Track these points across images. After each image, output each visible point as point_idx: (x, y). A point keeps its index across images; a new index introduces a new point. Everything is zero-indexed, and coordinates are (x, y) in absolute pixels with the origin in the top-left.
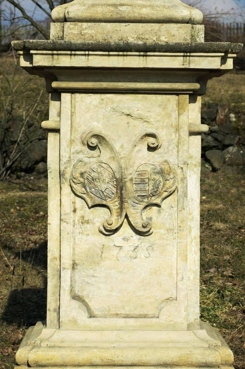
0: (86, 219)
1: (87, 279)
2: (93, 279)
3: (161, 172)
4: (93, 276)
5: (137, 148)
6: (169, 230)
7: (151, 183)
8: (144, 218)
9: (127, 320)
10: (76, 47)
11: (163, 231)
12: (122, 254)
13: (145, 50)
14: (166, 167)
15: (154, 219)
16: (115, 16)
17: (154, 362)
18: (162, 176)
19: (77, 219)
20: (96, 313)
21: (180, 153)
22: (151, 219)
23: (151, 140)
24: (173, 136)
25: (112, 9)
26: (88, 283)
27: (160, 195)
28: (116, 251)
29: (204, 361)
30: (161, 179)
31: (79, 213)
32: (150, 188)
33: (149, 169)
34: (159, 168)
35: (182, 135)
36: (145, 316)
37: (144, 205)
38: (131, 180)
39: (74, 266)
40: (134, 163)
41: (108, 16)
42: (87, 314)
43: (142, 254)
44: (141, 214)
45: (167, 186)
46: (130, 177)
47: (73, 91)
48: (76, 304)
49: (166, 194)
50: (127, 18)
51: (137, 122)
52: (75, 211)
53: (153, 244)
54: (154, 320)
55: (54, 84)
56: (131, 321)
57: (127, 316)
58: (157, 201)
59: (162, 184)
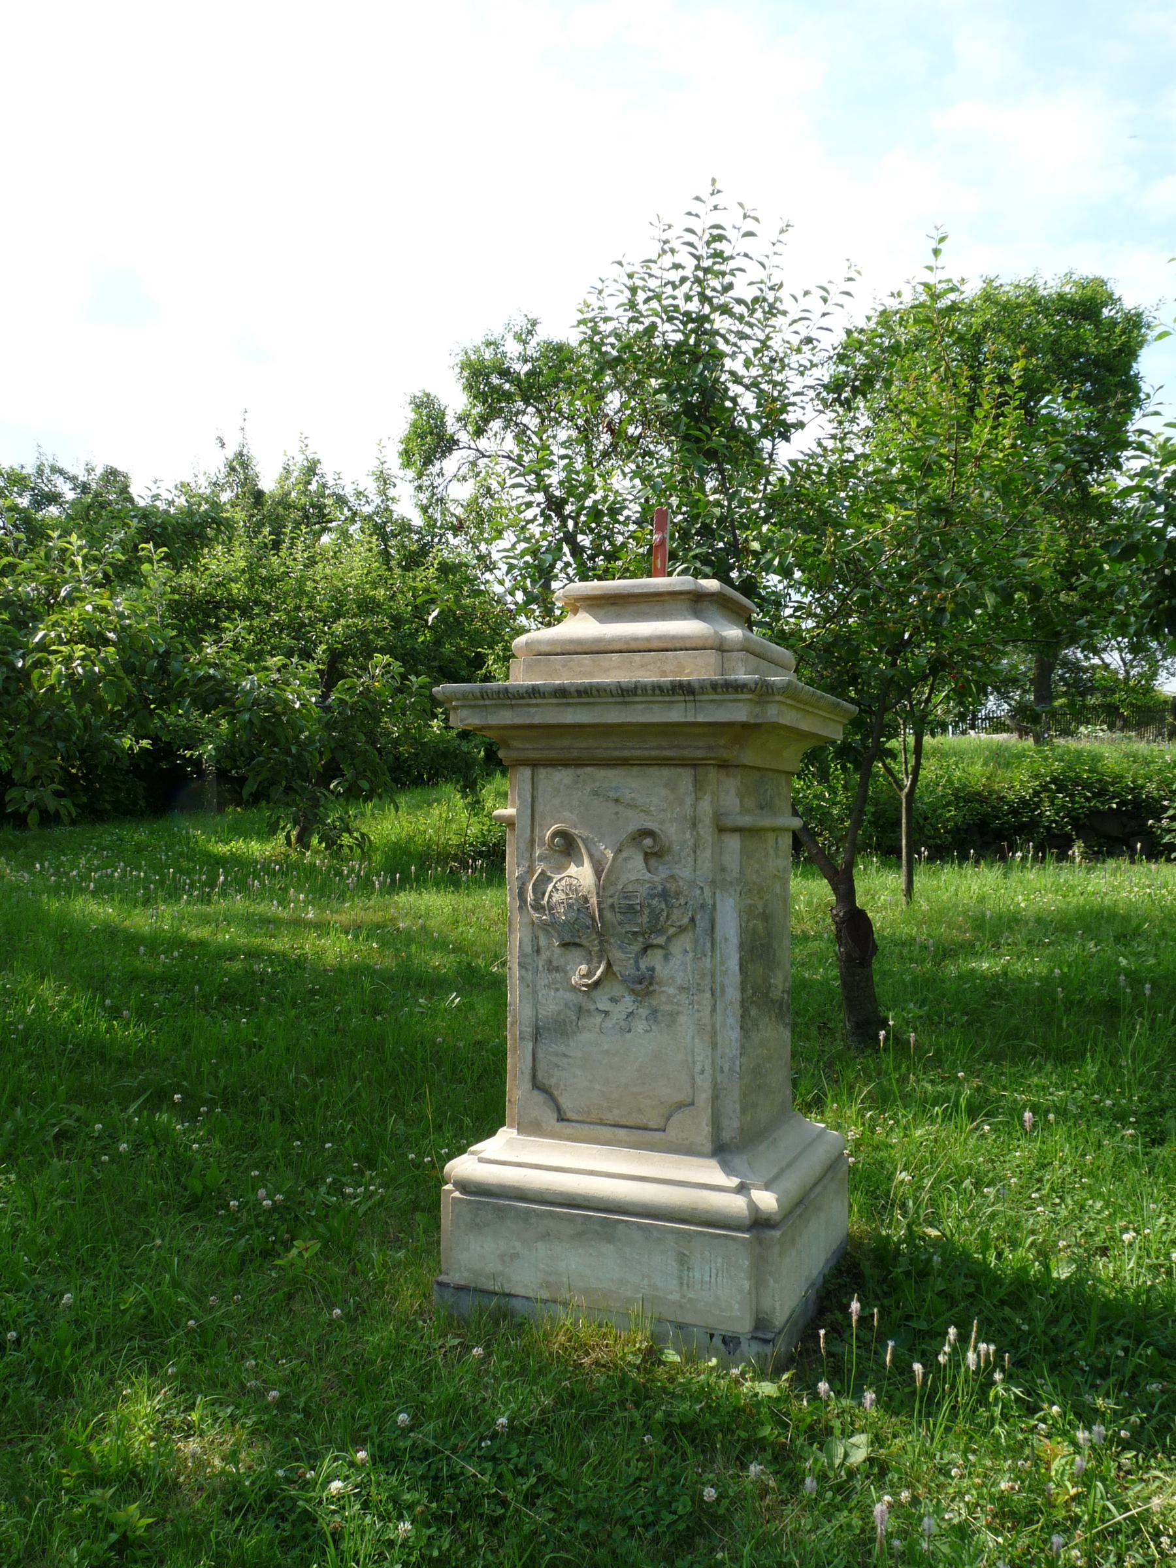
0: (555, 964)
1: (554, 1059)
2: (565, 1060)
3: (664, 895)
4: (565, 1056)
5: (625, 854)
6: (682, 989)
8: (643, 966)
10: (151, 675)
11: (671, 990)
12: (609, 1024)
14: (671, 887)
15: (658, 968)
18: (666, 901)
19: (541, 964)
20: (570, 1115)
21: (699, 862)
22: (652, 969)
23: (648, 842)
24: (688, 836)
26: (557, 1066)
28: (598, 1019)
31: (545, 955)
33: (643, 890)
34: (660, 888)
35: (702, 832)
39: (537, 1035)
40: (618, 879)
42: (555, 1115)
43: (640, 1026)
44: (637, 962)
45: (674, 917)
51: (630, 813)
52: (538, 951)
53: (656, 1011)
54: (658, 1135)
58: (661, 940)
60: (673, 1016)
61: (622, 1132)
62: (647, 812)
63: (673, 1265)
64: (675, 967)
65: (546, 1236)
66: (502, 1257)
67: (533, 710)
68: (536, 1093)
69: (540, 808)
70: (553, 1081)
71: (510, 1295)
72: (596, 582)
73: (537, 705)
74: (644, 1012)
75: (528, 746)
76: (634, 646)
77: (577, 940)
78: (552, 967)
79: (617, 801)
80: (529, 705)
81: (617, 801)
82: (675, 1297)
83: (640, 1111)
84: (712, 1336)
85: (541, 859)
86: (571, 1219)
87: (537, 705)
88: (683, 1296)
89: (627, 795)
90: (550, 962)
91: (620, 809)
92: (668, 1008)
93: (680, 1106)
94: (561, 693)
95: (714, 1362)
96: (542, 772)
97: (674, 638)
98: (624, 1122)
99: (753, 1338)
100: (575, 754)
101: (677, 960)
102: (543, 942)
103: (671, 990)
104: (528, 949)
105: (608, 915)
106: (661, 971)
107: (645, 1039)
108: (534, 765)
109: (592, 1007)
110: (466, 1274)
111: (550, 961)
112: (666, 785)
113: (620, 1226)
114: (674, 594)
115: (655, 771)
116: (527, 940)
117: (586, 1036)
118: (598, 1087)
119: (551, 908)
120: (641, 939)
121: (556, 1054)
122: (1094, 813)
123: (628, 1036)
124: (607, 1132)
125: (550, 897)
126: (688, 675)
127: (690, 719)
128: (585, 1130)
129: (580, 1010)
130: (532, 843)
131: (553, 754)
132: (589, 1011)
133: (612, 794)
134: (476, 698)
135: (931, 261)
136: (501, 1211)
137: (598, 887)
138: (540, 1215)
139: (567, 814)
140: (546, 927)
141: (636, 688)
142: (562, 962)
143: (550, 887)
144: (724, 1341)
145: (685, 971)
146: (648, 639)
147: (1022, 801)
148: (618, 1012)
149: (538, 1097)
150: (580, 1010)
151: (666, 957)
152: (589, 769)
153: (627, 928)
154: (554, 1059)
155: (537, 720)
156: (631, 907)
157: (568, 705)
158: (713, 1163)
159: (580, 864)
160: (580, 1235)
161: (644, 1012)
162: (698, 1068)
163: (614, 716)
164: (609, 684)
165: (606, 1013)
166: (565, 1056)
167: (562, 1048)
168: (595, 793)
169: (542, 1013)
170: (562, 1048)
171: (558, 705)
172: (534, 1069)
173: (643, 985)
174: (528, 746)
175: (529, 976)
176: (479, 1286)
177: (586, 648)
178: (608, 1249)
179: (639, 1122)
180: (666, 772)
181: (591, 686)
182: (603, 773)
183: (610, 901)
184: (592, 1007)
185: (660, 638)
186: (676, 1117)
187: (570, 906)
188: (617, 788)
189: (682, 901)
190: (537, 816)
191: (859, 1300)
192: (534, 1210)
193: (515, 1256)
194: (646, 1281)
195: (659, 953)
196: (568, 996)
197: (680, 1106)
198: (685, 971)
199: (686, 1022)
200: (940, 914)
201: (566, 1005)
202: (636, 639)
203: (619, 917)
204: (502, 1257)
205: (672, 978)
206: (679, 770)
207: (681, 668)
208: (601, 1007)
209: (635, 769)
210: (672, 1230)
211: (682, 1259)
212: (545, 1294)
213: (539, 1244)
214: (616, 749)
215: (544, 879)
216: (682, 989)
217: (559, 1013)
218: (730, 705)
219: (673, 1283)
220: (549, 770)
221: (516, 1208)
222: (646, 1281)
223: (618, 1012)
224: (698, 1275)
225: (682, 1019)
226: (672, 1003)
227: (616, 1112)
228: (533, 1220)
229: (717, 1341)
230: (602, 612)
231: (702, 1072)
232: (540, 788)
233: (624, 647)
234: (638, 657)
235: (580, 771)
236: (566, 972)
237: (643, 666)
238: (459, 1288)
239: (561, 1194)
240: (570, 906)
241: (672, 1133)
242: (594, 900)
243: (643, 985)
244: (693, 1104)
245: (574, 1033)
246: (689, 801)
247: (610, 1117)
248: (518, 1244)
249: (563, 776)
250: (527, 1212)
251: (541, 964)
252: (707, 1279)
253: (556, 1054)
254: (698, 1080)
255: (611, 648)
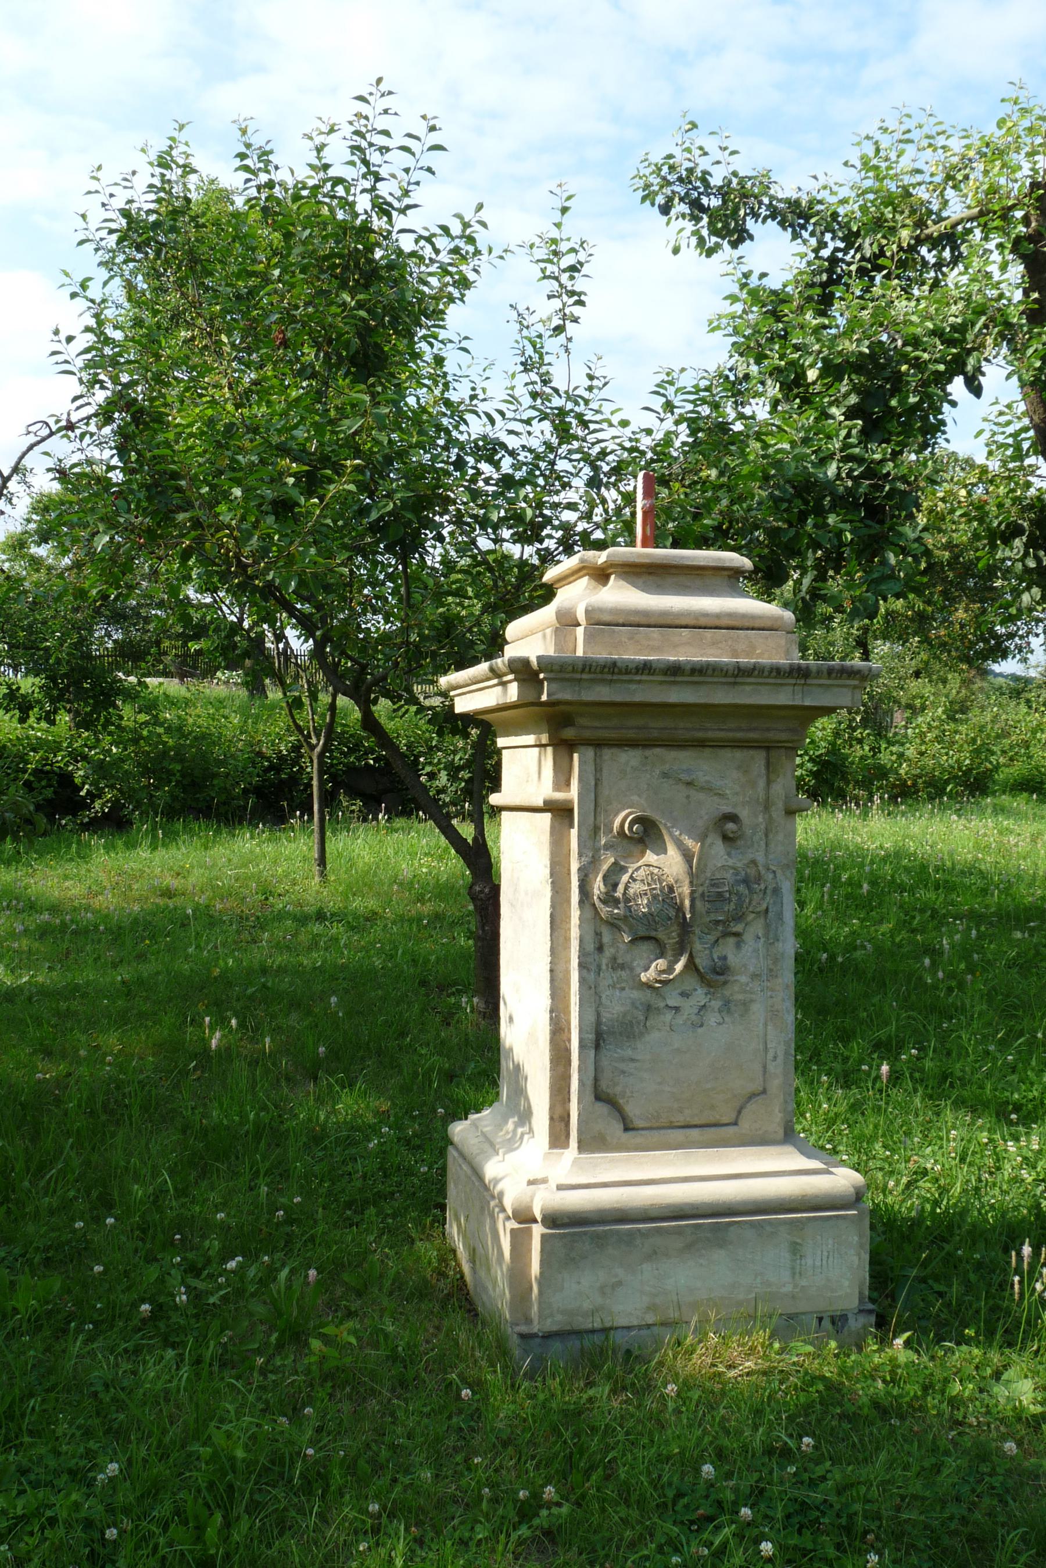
0: (620, 961)
1: (622, 1066)
2: (632, 1065)
4: (632, 1060)
6: (755, 976)
12: (680, 1020)
19: (604, 961)
21: (772, 846)
24: (761, 820)
28: (668, 1016)
31: (609, 952)
35: (774, 815)
43: (712, 1019)
45: (754, 903)
51: (701, 796)
54: (731, 1130)
60: (746, 1005)
61: (695, 1133)
62: (721, 796)
63: (786, 1256)
64: (746, 957)
65: (652, 1256)
66: (602, 1290)
67: (633, 687)
68: (599, 1104)
69: (605, 792)
70: (618, 1089)
71: (605, 1331)
72: (734, 555)
73: (639, 682)
74: (716, 1004)
75: (597, 724)
76: (703, 621)
77: (653, 934)
78: (616, 965)
79: (689, 784)
80: (630, 681)
81: (689, 784)
82: (788, 1288)
83: (713, 1107)
84: (820, 1319)
85: (608, 847)
86: (679, 1231)
87: (639, 682)
88: (795, 1286)
89: (701, 778)
90: (614, 959)
91: (692, 792)
92: (740, 997)
93: (753, 1096)
94: (674, 670)
95: (833, 1344)
96: (607, 753)
97: (744, 616)
98: (696, 1121)
99: (861, 1311)
100: (655, 734)
101: (748, 948)
102: (606, 939)
103: (743, 979)
104: (591, 947)
105: (699, 904)
106: (733, 960)
107: (718, 1032)
108: (598, 744)
109: (662, 1005)
110: (559, 1317)
111: (614, 959)
112: (739, 768)
113: (732, 1228)
114: (718, 570)
115: (727, 753)
116: (590, 938)
117: (654, 1036)
118: (667, 1089)
119: (627, 899)
120: (720, 928)
121: (623, 1060)
122: (351, 769)
123: (700, 1030)
124: (678, 1135)
125: (626, 888)
126: (760, 656)
127: (798, 702)
128: (655, 1136)
129: (649, 1008)
130: (596, 830)
131: (631, 734)
132: (658, 1009)
133: (685, 777)
134: (574, 671)
135: (557, 217)
136: (600, 1241)
137: (691, 874)
138: (644, 1234)
139: (635, 798)
140: (613, 924)
141: (754, 669)
142: (628, 958)
143: (625, 878)
144: (833, 1323)
145: (758, 958)
146: (718, 616)
147: (281, 758)
148: (689, 1007)
149: (602, 1108)
150: (649, 1008)
151: (738, 946)
152: (657, 751)
153: (713, 917)
154: (622, 1066)
155: (638, 698)
156: (720, 895)
157: (674, 683)
158: (790, 1149)
159: (662, 850)
160: (689, 1247)
161: (716, 1004)
162: (770, 1055)
163: (722, 696)
164: (727, 664)
165: (677, 1009)
166: (632, 1060)
167: (629, 1053)
168: (665, 775)
169: (606, 1016)
170: (629, 1053)
171: (661, 683)
172: (596, 1080)
173: (713, 977)
174: (597, 724)
175: (592, 976)
176: (576, 1327)
177: (652, 621)
178: (719, 1255)
179: (712, 1120)
180: (739, 754)
181: (708, 664)
182: (673, 754)
183: (700, 890)
184: (662, 1005)
185: (730, 615)
186: (751, 1107)
187: (655, 897)
188: (688, 771)
189: (762, 886)
190: (601, 801)
191: (1030, 1245)
192: (639, 1230)
193: (620, 1283)
194: (758, 1280)
195: (731, 940)
196: (636, 994)
197: (753, 1096)
198: (758, 958)
199: (758, 1009)
200: (364, 883)
201: (633, 1003)
202: (706, 615)
203: (708, 905)
204: (602, 1290)
205: (745, 966)
206: (752, 752)
207: (751, 650)
208: (671, 1003)
209: (708, 750)
210: (785, 1222)
211: (795, 1249)
212: (650, 1319)
213: (644, 1266)
214: (750, 730)
215: (617, 869)
216: (755, 976)
217: (625, 1014)
218: (836, 690)
219: (786, 1276)
220: (615, 750)
221: (618, 1231)
222: (758, 1280)
223: (689, 1007)
224: (810, 1262)
225: (755, 1007)
226: (745, 992)
227: (687, 1112)
228: (638, 1242)
229: (827, 1323)
230: (640, 581)
231: (775, 1058)
232: (605, 772)
233: (692, 622)
234: (709, 634)
235: (648, 752)
236: (632, 969)
237: (714, 643)
238: (548, 1336)
239: (668, 1206)
240: (655, 897)
241: (746, 1125)
242: (686, 890)
243: (713, 977)
244: (764, 1092)
245: (641, 1034)
246: (762, 783)
247: (680, 1119)
248: (620, 1271)
249: (630, 758)
250: (631, 1234)
251: (604, 961)
252: (818, 1263)
253: (623, 1060)
254: (771, 1067)
255: (678, 622)
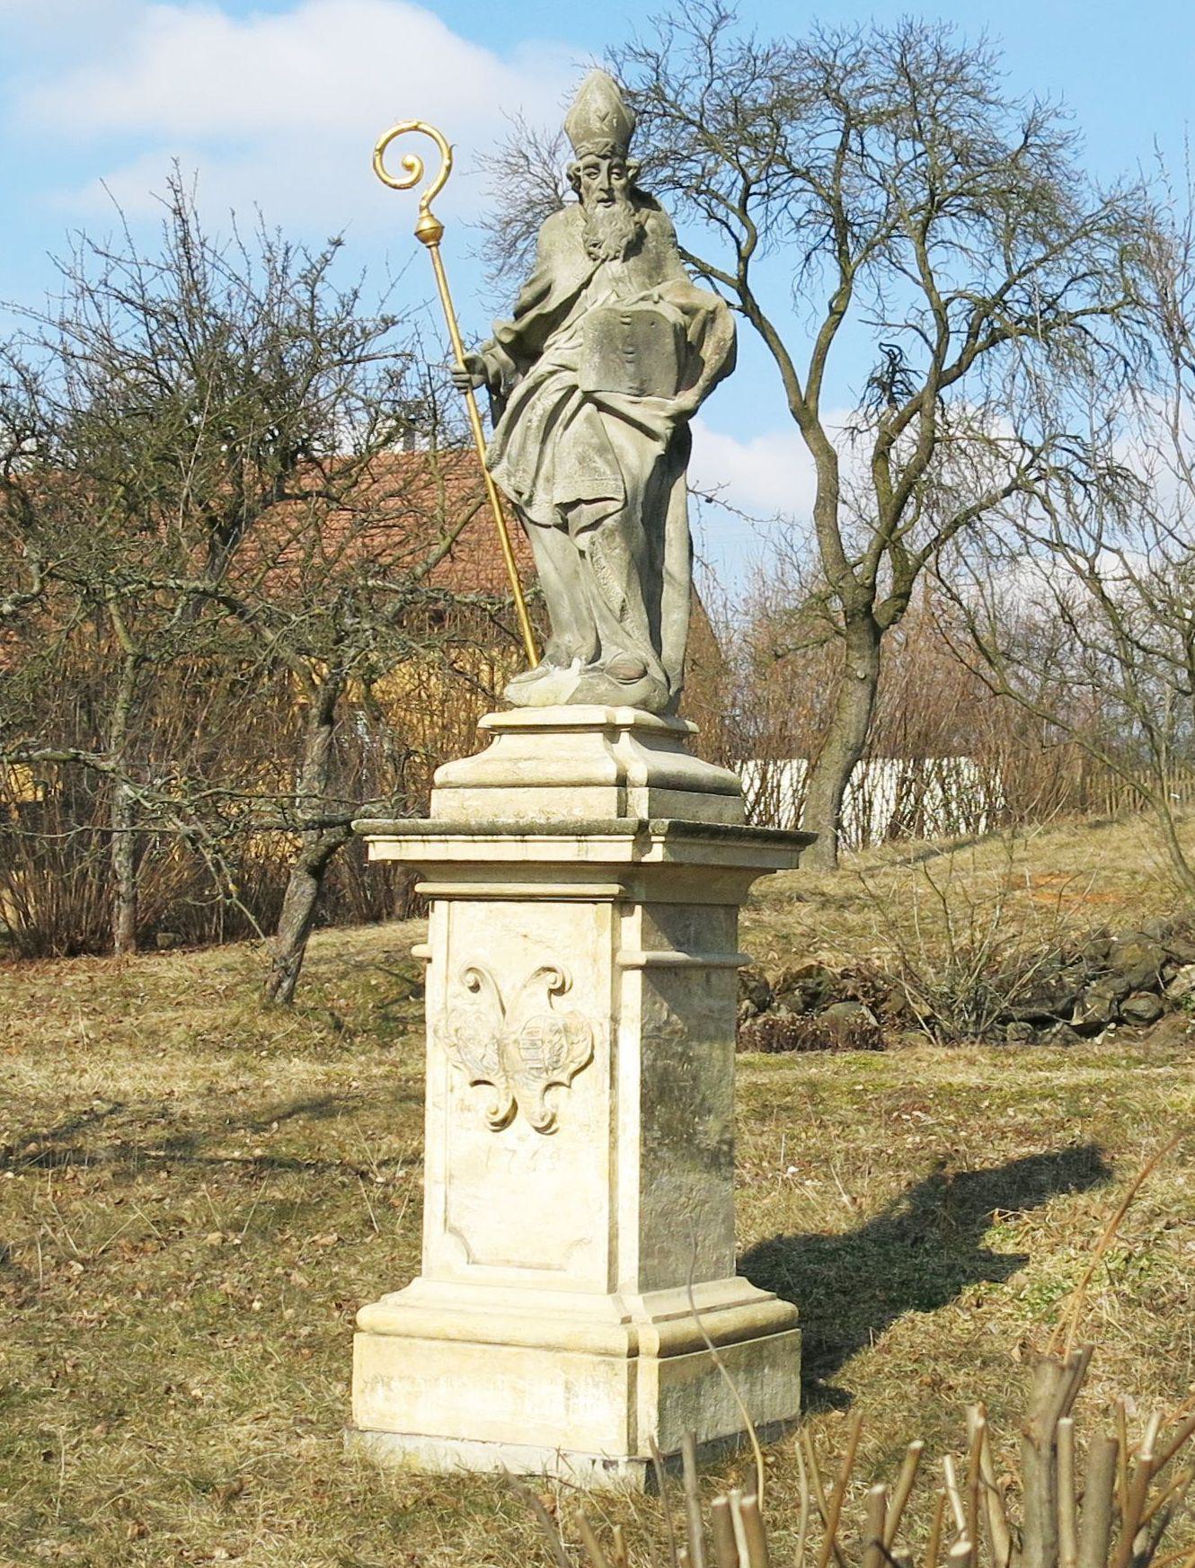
5: (529, 990)
7: (547, 1047)
9: (523, 1271)
13: (523, 832)
16: (512, 778)
17: (532, 1342)
20: (478, 1256)
25: (508, 765)
27: (564, 1068)
29: (602, 1345)
30: (564, 1041)
32: (545, 1055)
36: (548, 1268)
37: (543, 1084)
38: (516, 1041)
39: (450, 1177)
41: (501, 778)
46: (513, 1037)
47: (450, 898)
48: (451, 1239)
49: (573, 1067)
50: (527, 780)
55: (419, 888)
56: (526, 1273)
57: (522, 1266)
59: (565, 1050)
